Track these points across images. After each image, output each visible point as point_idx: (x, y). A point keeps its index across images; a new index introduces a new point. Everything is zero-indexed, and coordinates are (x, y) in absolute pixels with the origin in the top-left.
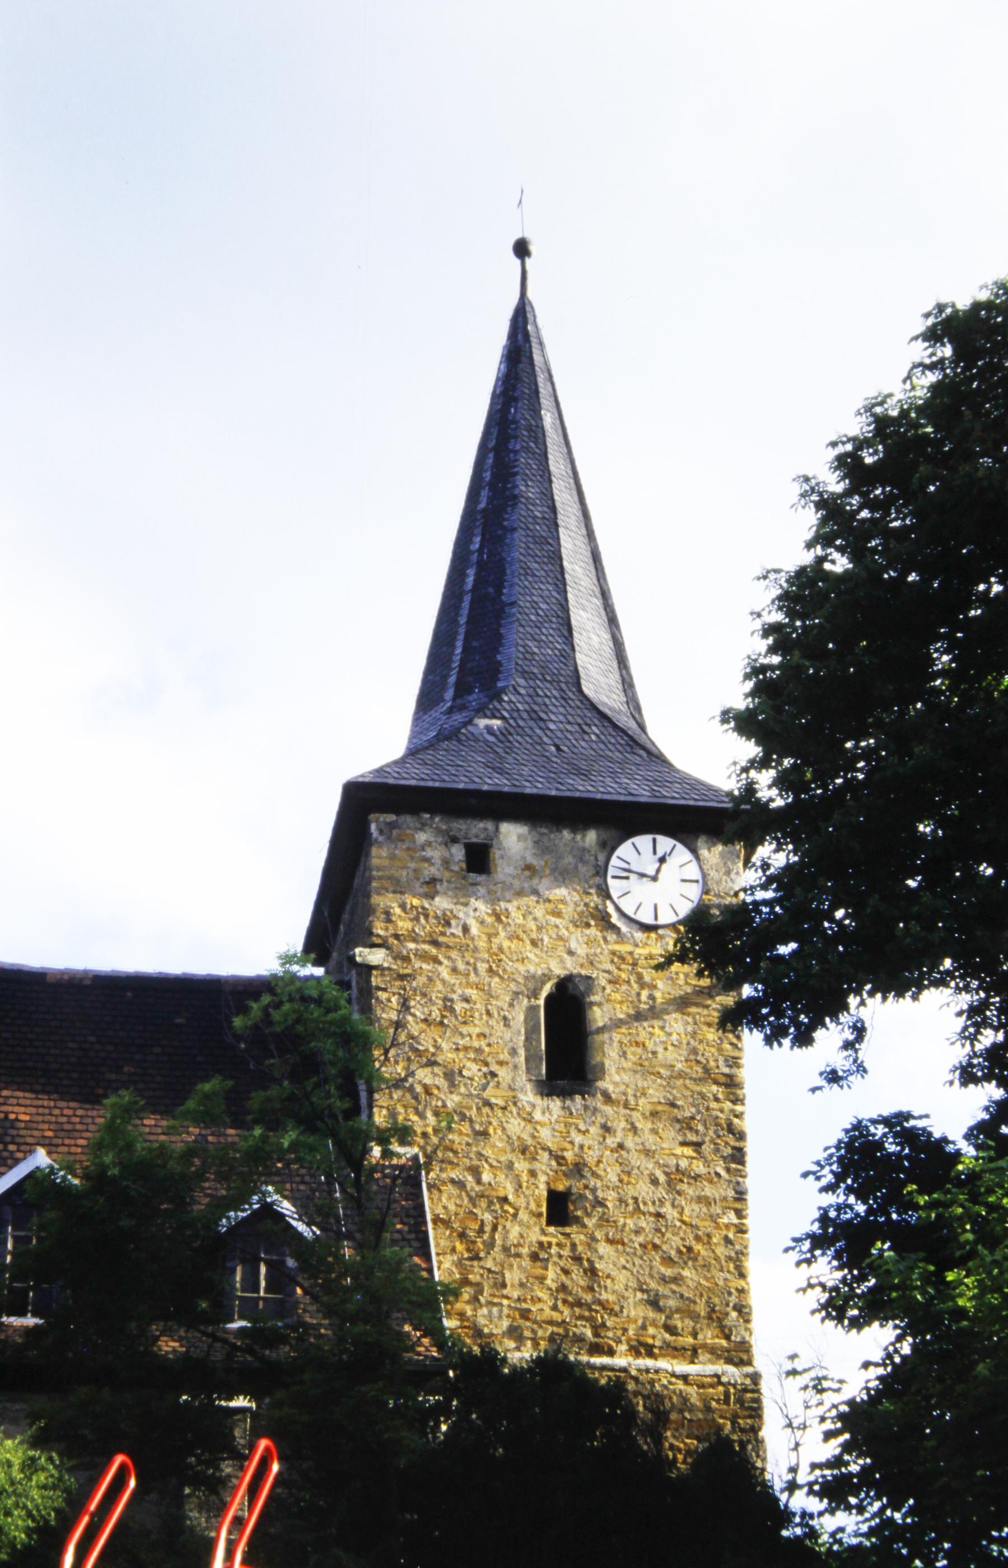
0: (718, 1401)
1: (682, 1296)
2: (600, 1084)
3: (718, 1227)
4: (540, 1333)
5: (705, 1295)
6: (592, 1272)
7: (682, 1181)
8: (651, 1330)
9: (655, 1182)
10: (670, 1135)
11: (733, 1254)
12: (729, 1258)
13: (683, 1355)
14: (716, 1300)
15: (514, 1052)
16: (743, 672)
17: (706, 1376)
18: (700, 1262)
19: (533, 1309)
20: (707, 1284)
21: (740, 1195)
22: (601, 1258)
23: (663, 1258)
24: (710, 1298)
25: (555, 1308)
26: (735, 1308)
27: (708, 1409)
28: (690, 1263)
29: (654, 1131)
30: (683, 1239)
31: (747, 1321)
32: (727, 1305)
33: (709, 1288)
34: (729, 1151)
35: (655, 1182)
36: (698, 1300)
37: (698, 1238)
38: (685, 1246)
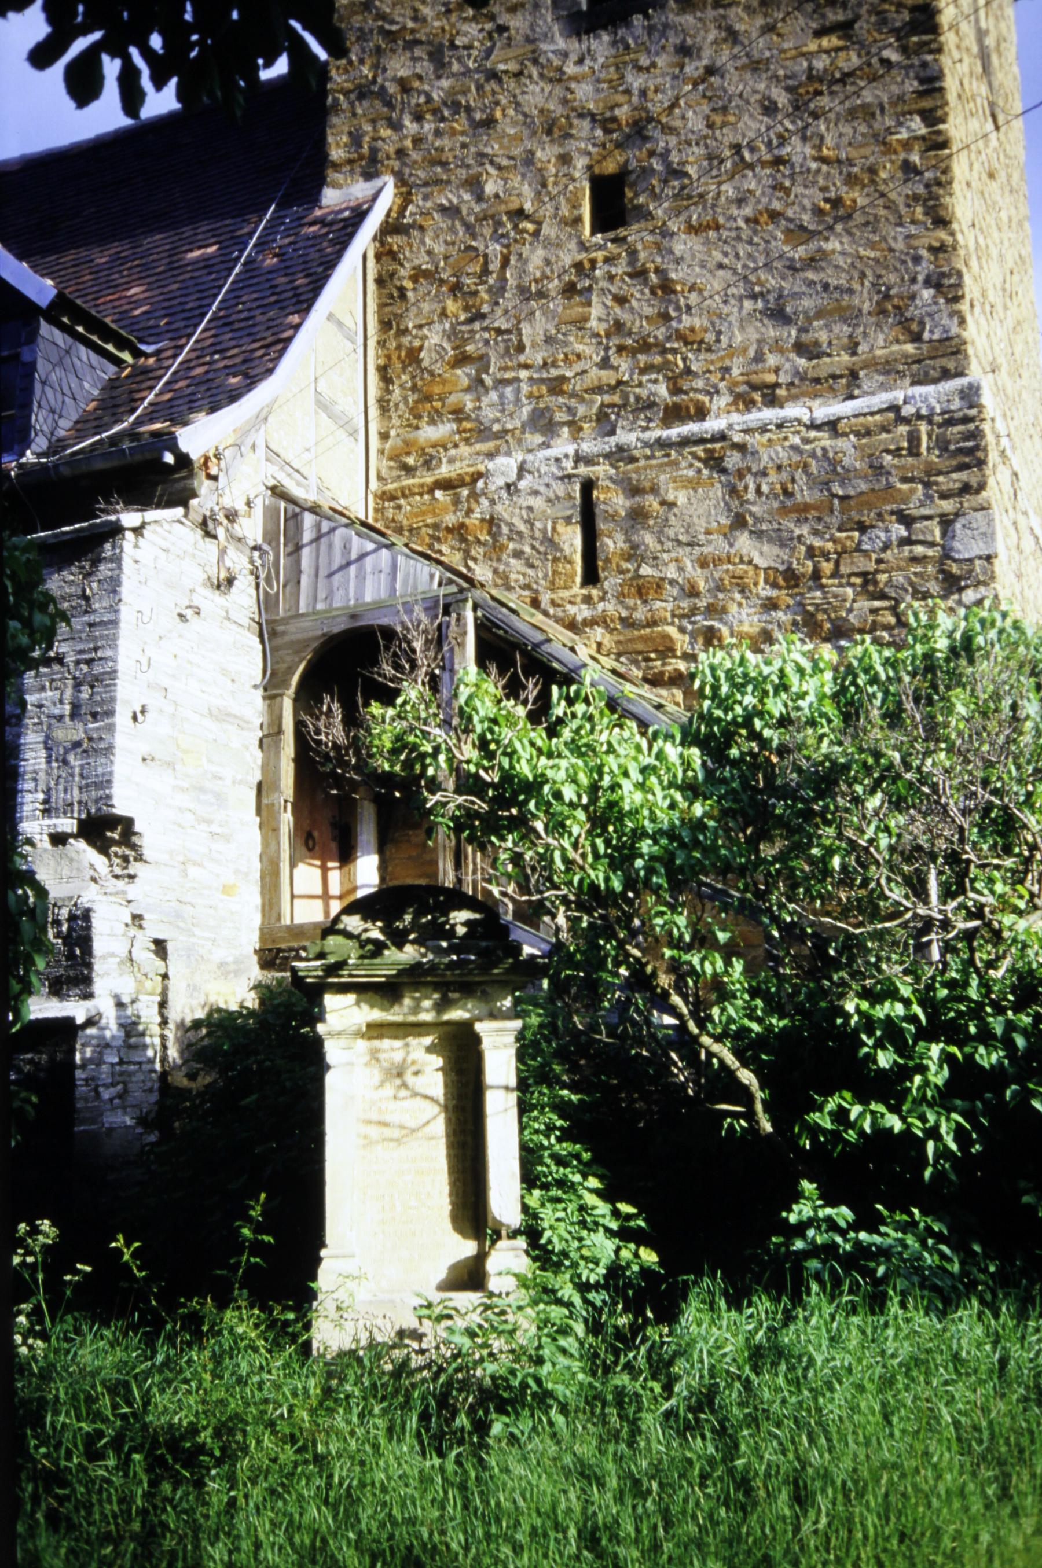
0: (896, 453)
1: (826, 287)
4: (581, 410)
5: (869, 273)
7: (819, 93)
9: (770, 108)
11: (921, 190)
14: (892, 278)
21: (931, 84)
22: (678, 261)
23: (788, 232)
25: (605, 364)
26: (928, 283)
27: (879, 470)
33: (877, 261)
34: (906, 16)
36: (856, 286)
37: (851, 180)
38: (827, 200)
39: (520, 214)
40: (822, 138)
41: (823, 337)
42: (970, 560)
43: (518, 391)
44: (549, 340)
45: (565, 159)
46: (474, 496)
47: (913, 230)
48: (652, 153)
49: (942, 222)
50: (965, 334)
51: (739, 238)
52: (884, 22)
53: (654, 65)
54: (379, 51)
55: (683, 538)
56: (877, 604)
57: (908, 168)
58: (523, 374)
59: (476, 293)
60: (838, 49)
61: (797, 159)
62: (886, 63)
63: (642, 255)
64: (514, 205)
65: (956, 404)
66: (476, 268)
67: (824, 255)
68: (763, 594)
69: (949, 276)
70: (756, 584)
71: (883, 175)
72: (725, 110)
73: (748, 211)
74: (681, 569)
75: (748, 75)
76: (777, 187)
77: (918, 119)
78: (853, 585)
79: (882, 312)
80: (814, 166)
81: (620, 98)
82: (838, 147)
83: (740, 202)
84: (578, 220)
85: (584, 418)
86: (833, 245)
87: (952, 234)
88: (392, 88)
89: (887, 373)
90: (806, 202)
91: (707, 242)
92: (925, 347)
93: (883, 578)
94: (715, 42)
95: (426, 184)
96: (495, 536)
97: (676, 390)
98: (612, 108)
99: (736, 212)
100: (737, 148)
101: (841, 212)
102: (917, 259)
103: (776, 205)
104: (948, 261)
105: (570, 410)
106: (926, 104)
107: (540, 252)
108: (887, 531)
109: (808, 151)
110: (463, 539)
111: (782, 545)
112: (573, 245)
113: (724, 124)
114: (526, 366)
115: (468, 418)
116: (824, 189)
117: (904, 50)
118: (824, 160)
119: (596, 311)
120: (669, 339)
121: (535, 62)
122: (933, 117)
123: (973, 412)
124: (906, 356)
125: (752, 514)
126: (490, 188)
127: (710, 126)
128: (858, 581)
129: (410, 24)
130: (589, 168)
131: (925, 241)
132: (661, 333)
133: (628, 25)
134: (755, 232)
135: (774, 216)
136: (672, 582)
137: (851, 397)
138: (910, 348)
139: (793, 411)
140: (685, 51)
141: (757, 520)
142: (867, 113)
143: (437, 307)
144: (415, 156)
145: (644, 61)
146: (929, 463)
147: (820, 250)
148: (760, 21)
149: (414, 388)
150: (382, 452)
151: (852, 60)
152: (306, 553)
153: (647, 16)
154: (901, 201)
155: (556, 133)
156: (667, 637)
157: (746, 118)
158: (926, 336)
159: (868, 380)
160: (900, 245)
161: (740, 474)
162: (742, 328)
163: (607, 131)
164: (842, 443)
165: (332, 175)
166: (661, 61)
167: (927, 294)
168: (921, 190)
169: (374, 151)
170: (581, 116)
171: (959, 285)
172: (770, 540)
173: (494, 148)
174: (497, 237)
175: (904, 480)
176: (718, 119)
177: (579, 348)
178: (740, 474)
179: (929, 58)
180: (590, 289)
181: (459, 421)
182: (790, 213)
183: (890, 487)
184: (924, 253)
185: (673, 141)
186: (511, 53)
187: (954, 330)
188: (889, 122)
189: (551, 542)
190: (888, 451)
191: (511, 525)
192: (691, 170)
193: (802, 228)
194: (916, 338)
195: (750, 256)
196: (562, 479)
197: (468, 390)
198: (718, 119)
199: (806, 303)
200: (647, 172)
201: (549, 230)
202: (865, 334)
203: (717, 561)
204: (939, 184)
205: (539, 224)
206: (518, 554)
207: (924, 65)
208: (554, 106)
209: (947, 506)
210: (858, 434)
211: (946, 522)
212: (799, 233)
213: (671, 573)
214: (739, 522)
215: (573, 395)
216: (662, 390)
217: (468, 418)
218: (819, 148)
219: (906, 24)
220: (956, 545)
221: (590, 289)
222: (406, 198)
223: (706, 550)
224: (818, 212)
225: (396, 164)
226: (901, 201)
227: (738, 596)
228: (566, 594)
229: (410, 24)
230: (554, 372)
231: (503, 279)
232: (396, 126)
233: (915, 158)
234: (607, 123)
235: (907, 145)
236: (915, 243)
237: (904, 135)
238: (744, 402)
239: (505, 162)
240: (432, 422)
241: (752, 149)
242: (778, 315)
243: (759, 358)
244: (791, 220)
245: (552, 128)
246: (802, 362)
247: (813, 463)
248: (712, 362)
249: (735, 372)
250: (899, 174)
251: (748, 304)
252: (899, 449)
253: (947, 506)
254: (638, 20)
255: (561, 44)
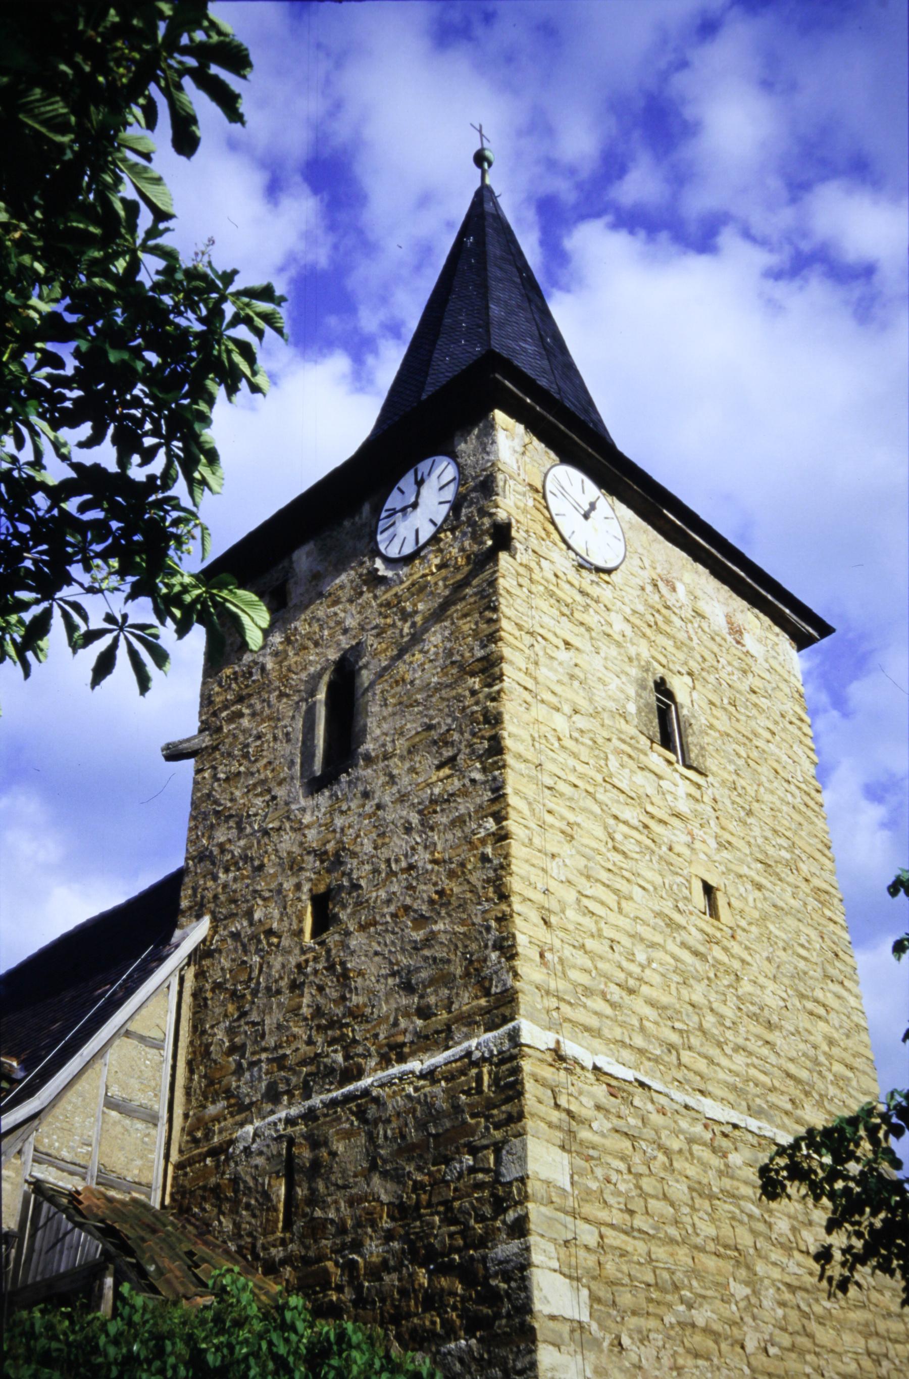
0: (467, 1093)
1: (434, 959)
2: (362, 750)
3: (472, 845)
4: (294, 1080)
5: (460, 945)
6: (344, 978)
7: (435, 812)
8: (403, 1023)
9: (408, 829)
10: (426, 761)
11: (491, 874)
12: (488, 881)
13: (436, 1043)
14: (474, 946)
15: (292, 763)
16: (899, 872)
17: (456, 1061)
18: (454, 902)
19: (288, 1052)
20: (461, 929)
21: (498, 793)
22: (352, 953)
23: (414, 920)
24: (466, 947)
25: (310, 1042)
26: (495, 947)
27: (457, 1109)
28: (443, 912)
29: (412, 770)
30: (435, 884)
31: (512, 957)
32: (486, 946)
33: (464, 934)
34: (486, 744)
35: (408, 829)
36: (452, 957)
37: (451, 875)
38: (437, 892)
39: (270, 933)
40: (435, 844)
41: (432, 1000)
42: (510, 1183)
43: (260, 1069)
44: (279, 1027)
45: (298, 887)
46: (227, 1160)
47: (486, 906)
48: (344, 874)
49: (504, 897)
50: (518, 985)
51: (387, 931)
52: (473, 752)
53: (349, 809)
54: (212, 827)
55: (340, 1182)
56: (452, 1228)
57: (485, 858)
58: (264, 1056)
59: (244, 996)
60: (448, 777)
61: (420, 864)
62: (473, 781)
63: (334, 952)
64: (267, 927)
65: (506, 1046)
66: (244, 977)
67: (433, 935)
68: (386, 1226)
69: (507, 939)
70: (381, 1218)
71: (469, 867)
72: (384, 833)
73: (392, 908)
74: (338, 1210)
75: (398, 806)
76: (410, 887)
77: (491, 820)
78: (438, 1213)
79: (467, 974)
80: (429, 867)
81: (330, 836)
82: (444, 850)
83: (389, 902)
84: (301, 931)
85: (296, 1087)
86: (439, 926)
87: (510, 906)
88: (216, 850)
89: (469, 1025)
90: (425, 896)
91: (370, 937)
92: (492, 999)
93: (456, 1204)
94: (383, 785)
95: (226, 918)
96: (236, 1191)
97: (347, 1057)
98: (324, 845)
99: (386, 910)
100: (388, 861)
101: (444, 900)
102: (488, 929)
103: (408, 901)
104: (507, 927)
105: (288, 1081)
106: (495, 808)
107: (280, 959)
108: (461, 1162)
109: (428, 856)
110: (218, 1198)
111: (399, 1182)
112: (297, 951)
113: (383, 844)
114: (265, 1050)
115: (233, 1096)
116: (435, 884)
117: (484, 770)
118: (435, 862)
119: (306, 1000)
120: (344, 1016)
121: (288, 818)
122: (499, 818)
123: (516, 1051)
124: (481, 1008)
125: (381, 1157)
126: (257, 915)
127: (375, 848)
128: (441, 1209)
129: (229, 804)
130: (311, 890)
131: (493, 914)
132: (339, 1011)
133: (338, 782)
134: (396, 923)
135: (407, 909)
136: (332, 1221)
137: (447, 1048)
138: (483, 1002)
139: (415, 1065)
140: (366, 795)
141: (385, 1161)
142: (460, 821)
143: (222, 1009)
144: (222, 898)
145: (344, 808)
146: (488, 1099)
147: (432, 932)
148: (407, 765)
149: (205, 1076)
150: (183, 1129)
151: (456, 784)
152: (40, 1233)
153: (349, 774)
154: (479, 885)
155: (296, 868)
156: (326, 1270)
157: (395, 838)
158: (493, 990)
159: (458, 1032)
160: (478, 920)
161: (376, 1122)
162: (387, 1002)
163: (322, 862)
164: (436, 1089)
165: (183, 920)
166: (353, 805)
167: (494, 956)
168: (491, 874)
169: (203, 897)
170: (309, 853)
171: (513, 946)
172: (392, 1179)
173: (261, 886)
174: (258, 951)
175: (473, 1116)
176: (380, 842)
177: (295, 1030)
178: (376, 1122)
179: (497, 773)
180: (303, 983)
181: (227, 1098)
182: (415, 907)
183: (464, 1122)
184: (493, 924)
185: (355, 862)
186: (277, 814)
187: (510, 982)
188: (474, 826)
189: (266, 1195)
190: (464, 1092)
191: (245, 1182)
192: (363, 883)
193: (422, 916)
194: (487, 993)
195: (393, 943)
196: (275, 1139)
197: (233, 1073)
198: (380, 842)
199: (424, 975)
200: (341, 887)
201: (286, 942)
202: (457, 994)
203: (361, 1199)
204: (502, 867)
205: (280, 937)
206: (248, 1207)
207: (495, 779)
208: (296, 849)
209: (498, 1135)
210: (447, 1080)
211: (498, 1148)
212: (421, 921)
213: (332, 1215)
214: (373, 1167)
215: (290, 1069)
216: (339, 1057)
217: (233, 1096)
218: (432, 853)
219: (487, 750)
220: (503, 1170)
221: (303, 983)
222: (214, 929)
223: (354, 1191)
224: (431, 902)
225: (212, 906)
226: (479, 885)
227: (369, 1230)
228: (271, 1238)
229: (229, 804)
230: (281, 1052)
231: (258, 983)
232: (215, 878)
233: (489, 850)
234: (321, 855)
235: (483, 841)
236: (487, 916)
237: (482, 833)
238: (385, 1062)
239: (267, 894)
240: (213, 1102)
241: (397, 861)
242: (408, 988)
243: (396, 1024)
244: (415, 911)
245: (294, 866)
246: (419, 1023)
247: (419, 1107)
248: (368, 1031)
249: (382, 1036)
250: (479, 865)
251: (390, 981)
252: (471, 1089)
253: (498, 1135)
254: (344, 777)
255: (303, 802)
